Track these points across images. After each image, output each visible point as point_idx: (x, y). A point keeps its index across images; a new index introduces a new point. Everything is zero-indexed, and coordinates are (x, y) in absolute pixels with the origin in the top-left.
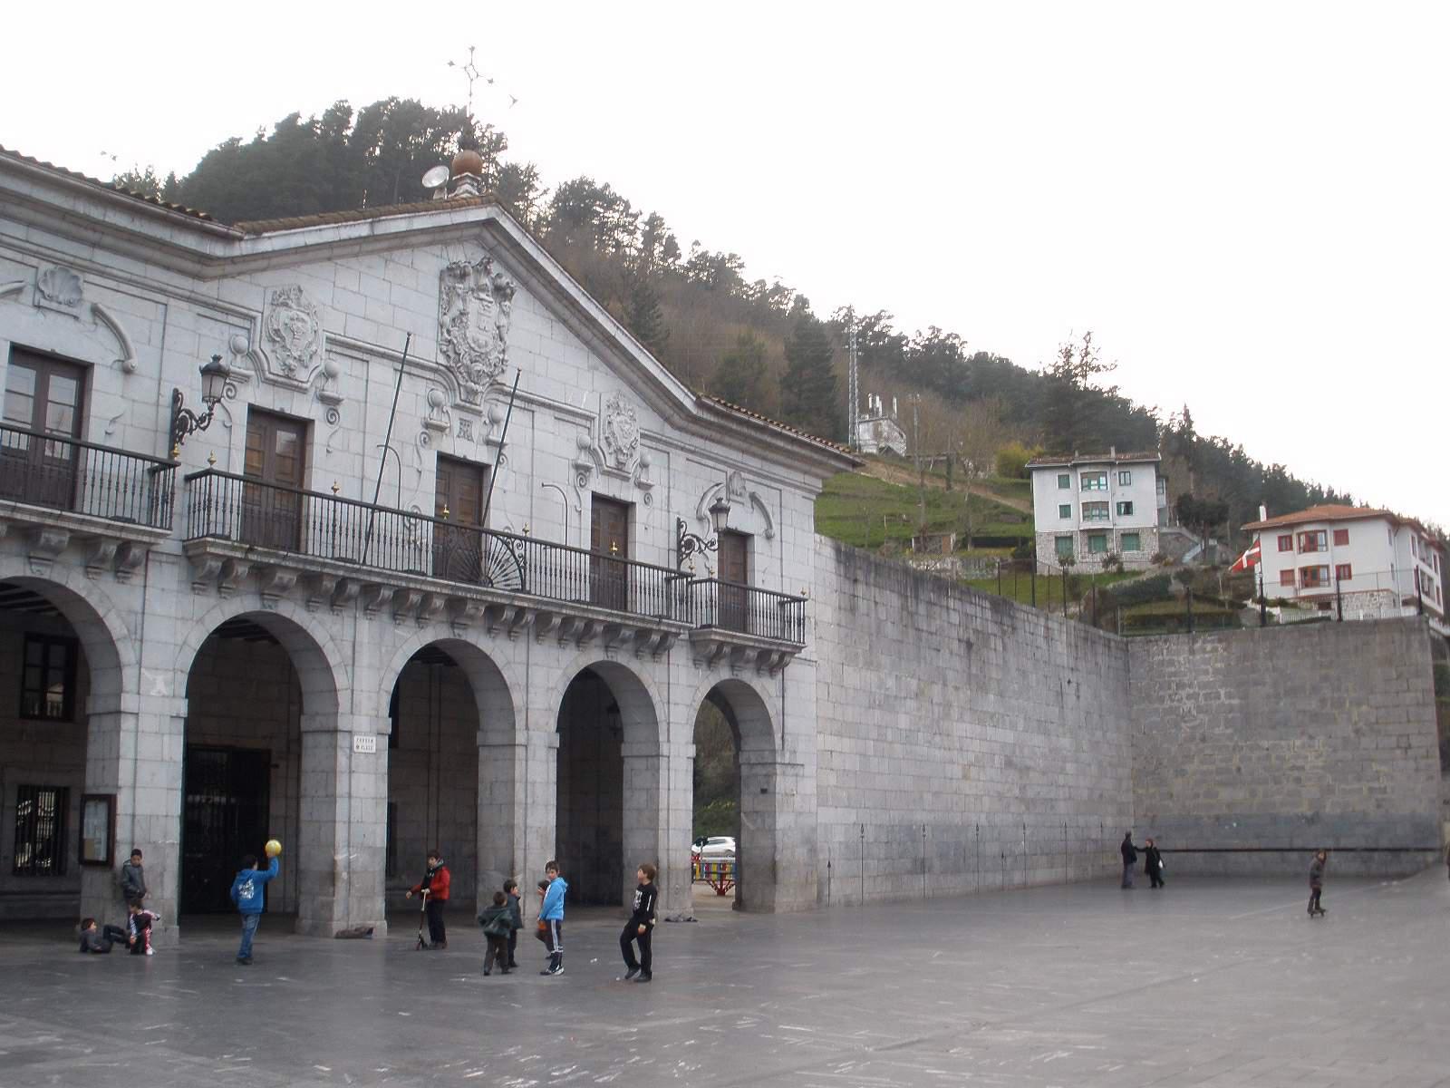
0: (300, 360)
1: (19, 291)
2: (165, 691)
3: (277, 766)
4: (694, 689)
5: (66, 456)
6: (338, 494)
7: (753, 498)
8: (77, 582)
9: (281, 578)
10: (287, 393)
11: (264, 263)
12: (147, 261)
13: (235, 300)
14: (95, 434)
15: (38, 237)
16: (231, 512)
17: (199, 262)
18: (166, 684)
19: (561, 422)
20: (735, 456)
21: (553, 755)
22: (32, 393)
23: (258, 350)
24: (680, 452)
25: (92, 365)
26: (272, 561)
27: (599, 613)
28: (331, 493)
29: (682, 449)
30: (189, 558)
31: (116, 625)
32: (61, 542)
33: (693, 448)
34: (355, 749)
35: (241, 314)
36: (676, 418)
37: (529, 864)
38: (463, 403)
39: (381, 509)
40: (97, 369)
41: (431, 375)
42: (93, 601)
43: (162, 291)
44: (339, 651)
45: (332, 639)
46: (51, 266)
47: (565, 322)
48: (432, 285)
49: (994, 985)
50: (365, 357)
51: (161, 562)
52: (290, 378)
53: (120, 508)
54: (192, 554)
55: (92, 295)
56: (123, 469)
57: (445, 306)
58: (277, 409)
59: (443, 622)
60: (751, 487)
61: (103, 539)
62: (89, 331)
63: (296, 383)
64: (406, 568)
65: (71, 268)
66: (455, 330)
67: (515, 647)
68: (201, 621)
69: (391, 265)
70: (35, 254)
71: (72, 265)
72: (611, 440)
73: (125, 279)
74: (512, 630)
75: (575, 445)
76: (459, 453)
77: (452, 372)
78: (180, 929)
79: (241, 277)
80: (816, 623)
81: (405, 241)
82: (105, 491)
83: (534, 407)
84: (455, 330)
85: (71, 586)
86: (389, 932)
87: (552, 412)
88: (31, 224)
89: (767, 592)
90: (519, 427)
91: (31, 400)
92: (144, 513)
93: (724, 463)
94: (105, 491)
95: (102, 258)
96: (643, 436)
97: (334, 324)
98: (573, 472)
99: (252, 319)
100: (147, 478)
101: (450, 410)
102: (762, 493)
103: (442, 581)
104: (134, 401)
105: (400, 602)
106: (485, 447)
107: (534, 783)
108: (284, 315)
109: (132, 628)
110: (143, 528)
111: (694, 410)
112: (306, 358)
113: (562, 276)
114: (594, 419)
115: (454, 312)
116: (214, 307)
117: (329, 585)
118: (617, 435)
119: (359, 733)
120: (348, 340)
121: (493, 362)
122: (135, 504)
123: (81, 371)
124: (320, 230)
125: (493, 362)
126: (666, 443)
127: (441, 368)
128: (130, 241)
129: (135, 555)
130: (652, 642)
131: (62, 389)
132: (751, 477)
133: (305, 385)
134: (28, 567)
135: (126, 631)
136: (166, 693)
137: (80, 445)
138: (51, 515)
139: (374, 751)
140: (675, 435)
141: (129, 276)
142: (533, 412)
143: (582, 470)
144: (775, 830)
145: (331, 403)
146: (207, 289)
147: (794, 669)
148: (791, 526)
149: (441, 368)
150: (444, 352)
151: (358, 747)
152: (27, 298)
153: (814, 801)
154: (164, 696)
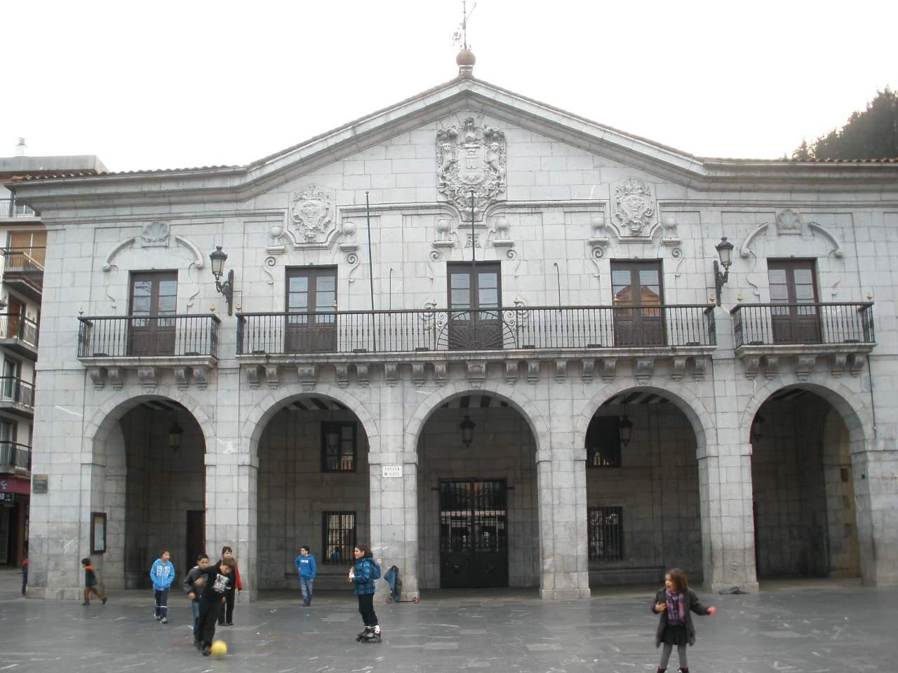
0: (316, 229)
1: (133, 241)
2: (233, 450)
3: (512, 488)
5: (814, 312)
6: (437, 307)
7: (814, 228)
8: (672, 387)
9: (302, 371)
11: (281, 179)
12: (204, 202)
13: (267, 207)
14: (825, 297)
16: (828, 326)
17: (233, 193)
18: (234, 446)
19: (573, 214)
21: (747, 462)
22: (785, 282)
23: (610, 225)
24: (713, 208)
26: (287, 362)
27: (812, 348)
28: (514, 305)
29: (714, 205)
30: (741, 359)
31: (199, 415)
32: (150, 373)
33: (726, 202)
34: (384, 476)
35: (276, 213)
36: (695, 183)
37: (558, 551)
38: (465, 223)
39: (341, 313)
41: (438, 211)
42: (184, 403)
43: (219, 216)
44: (368, 411)
45: (362, 403)
46: (150, 223)
47: (563, 141)
48: (431, 151)
51: (226, 374)
52: (312, 243)
53: (593, 339)
54: (739, 357)
55: (175, 232)
56: (758, 315)
57: (440, 160)
59: (462, 380)
60: (806, 219)
61: (675, 358)
62: (175, 252)
63: (317, 245)
64: (750, 341)
65: (160, 221)
67: (536, 388)
68: (258, 405)
69: (391, 148)
71: (161, 219)
72: (622, 216)
73: (193, 216)
74: (533, 378)
75: (590, 227)
76: (459, 259)
77: (452, 205)
78: (759, 584)
79: (271, 192)
81: (396, 130)
82: (198, 340)
83: (542, 210)
86: (761, 587)
87: (561, 209)
88: (131, 205)
89: (841, 304)
90: (521, 228)
91: (786, 286)
92: (862, 335)
93: (770, 206)
94: (198, 340)
95: (176, 209)
96: (663, 205)
97: (346, 200)
98: (589, 248)
99: (282, 214)
100: (706, 317)
102: (824, 222)
103: (797, 346)
104: (205, 284)
105: (586, 365)
106: (494, 249)
107: (560, 489)
108: (300, 205)
109: (211, 416)
110: (121, 358)
111: (704, 173)
112: (322, 228)
113: (540, 110)
114: (605, 204)
115: (446, 164)
116: (254, 215)
117: (841, 359)
118: (626, 211)
119: (387, 464)
120: (359, 207)
121: (487, 188)
122: (701, 336)
123: (811, 263)
124: (311, 146)
125: (487, 188)
126: (692, 205)
127: (442, 204)
128: (186, 195)
129: (196, 373)
131: (802, 275)
133: (649, 239)
134: (470, 385)
135: (207, 418)
136: (234, 451)
137: (797, 306)
138: (134, 360)
139: (401, 475)
140: (702, 196)
141: (194, 214)
142: (699, 212)
144: (870, 511)
145: (351, 251)
148: (870, 241)
149: (442, 204)
151: (386, 474)
152: (137, 245)
154: (233, 453)
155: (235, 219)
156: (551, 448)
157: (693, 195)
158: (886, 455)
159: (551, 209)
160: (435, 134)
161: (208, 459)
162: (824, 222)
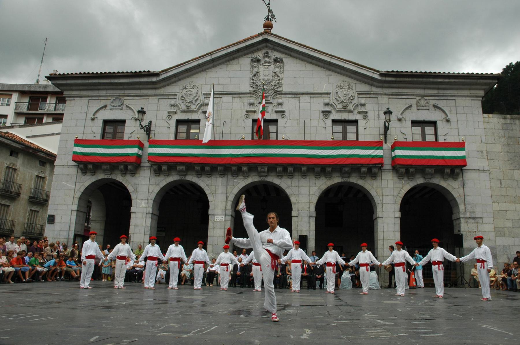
0: (191, 102)
1: (106, 106)
4: (399, 189)
10: (190, 114)
15: (109, 92)
20: (418, 91)
21: (398, 221)
25: (104, 120)
40: (438, 122)
41: (249, 95)
49: (32, 292)
50: (221, 96)
55: (126, 102)
58: (186, 119)
60: (432, 102)
65: (118, 97)
66: (255, 79)
70: (109, 96)
71: (120, 96)
74: (291, 176)
80: (487, 153)
84: (255, 79)
85: (118, 179)
90: (289, 104)
95: (127, 92)
101: (258, 105)
112: (194, 102)
115: (254, 73)
123: (434, 124)
125: (273, 85)
126: (374, 94)
130: (133, 166)
131: (430, 130)
132: (430, 98)
143: (326, 113)
146: (161, 91)
147: (468, 176)
150: (252, 87)
152: (109, 107)
153: (493, 234)
155: (155, 97)
156: (298, 210)
157: (375, 90)
158: (471, 220)
159: (304, 95)
160: (250, 59)
161: (132, 209)
162: (441, 104)
